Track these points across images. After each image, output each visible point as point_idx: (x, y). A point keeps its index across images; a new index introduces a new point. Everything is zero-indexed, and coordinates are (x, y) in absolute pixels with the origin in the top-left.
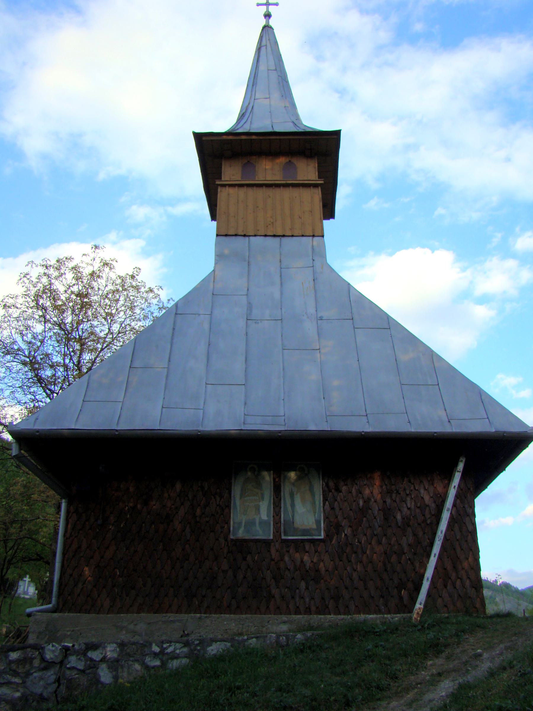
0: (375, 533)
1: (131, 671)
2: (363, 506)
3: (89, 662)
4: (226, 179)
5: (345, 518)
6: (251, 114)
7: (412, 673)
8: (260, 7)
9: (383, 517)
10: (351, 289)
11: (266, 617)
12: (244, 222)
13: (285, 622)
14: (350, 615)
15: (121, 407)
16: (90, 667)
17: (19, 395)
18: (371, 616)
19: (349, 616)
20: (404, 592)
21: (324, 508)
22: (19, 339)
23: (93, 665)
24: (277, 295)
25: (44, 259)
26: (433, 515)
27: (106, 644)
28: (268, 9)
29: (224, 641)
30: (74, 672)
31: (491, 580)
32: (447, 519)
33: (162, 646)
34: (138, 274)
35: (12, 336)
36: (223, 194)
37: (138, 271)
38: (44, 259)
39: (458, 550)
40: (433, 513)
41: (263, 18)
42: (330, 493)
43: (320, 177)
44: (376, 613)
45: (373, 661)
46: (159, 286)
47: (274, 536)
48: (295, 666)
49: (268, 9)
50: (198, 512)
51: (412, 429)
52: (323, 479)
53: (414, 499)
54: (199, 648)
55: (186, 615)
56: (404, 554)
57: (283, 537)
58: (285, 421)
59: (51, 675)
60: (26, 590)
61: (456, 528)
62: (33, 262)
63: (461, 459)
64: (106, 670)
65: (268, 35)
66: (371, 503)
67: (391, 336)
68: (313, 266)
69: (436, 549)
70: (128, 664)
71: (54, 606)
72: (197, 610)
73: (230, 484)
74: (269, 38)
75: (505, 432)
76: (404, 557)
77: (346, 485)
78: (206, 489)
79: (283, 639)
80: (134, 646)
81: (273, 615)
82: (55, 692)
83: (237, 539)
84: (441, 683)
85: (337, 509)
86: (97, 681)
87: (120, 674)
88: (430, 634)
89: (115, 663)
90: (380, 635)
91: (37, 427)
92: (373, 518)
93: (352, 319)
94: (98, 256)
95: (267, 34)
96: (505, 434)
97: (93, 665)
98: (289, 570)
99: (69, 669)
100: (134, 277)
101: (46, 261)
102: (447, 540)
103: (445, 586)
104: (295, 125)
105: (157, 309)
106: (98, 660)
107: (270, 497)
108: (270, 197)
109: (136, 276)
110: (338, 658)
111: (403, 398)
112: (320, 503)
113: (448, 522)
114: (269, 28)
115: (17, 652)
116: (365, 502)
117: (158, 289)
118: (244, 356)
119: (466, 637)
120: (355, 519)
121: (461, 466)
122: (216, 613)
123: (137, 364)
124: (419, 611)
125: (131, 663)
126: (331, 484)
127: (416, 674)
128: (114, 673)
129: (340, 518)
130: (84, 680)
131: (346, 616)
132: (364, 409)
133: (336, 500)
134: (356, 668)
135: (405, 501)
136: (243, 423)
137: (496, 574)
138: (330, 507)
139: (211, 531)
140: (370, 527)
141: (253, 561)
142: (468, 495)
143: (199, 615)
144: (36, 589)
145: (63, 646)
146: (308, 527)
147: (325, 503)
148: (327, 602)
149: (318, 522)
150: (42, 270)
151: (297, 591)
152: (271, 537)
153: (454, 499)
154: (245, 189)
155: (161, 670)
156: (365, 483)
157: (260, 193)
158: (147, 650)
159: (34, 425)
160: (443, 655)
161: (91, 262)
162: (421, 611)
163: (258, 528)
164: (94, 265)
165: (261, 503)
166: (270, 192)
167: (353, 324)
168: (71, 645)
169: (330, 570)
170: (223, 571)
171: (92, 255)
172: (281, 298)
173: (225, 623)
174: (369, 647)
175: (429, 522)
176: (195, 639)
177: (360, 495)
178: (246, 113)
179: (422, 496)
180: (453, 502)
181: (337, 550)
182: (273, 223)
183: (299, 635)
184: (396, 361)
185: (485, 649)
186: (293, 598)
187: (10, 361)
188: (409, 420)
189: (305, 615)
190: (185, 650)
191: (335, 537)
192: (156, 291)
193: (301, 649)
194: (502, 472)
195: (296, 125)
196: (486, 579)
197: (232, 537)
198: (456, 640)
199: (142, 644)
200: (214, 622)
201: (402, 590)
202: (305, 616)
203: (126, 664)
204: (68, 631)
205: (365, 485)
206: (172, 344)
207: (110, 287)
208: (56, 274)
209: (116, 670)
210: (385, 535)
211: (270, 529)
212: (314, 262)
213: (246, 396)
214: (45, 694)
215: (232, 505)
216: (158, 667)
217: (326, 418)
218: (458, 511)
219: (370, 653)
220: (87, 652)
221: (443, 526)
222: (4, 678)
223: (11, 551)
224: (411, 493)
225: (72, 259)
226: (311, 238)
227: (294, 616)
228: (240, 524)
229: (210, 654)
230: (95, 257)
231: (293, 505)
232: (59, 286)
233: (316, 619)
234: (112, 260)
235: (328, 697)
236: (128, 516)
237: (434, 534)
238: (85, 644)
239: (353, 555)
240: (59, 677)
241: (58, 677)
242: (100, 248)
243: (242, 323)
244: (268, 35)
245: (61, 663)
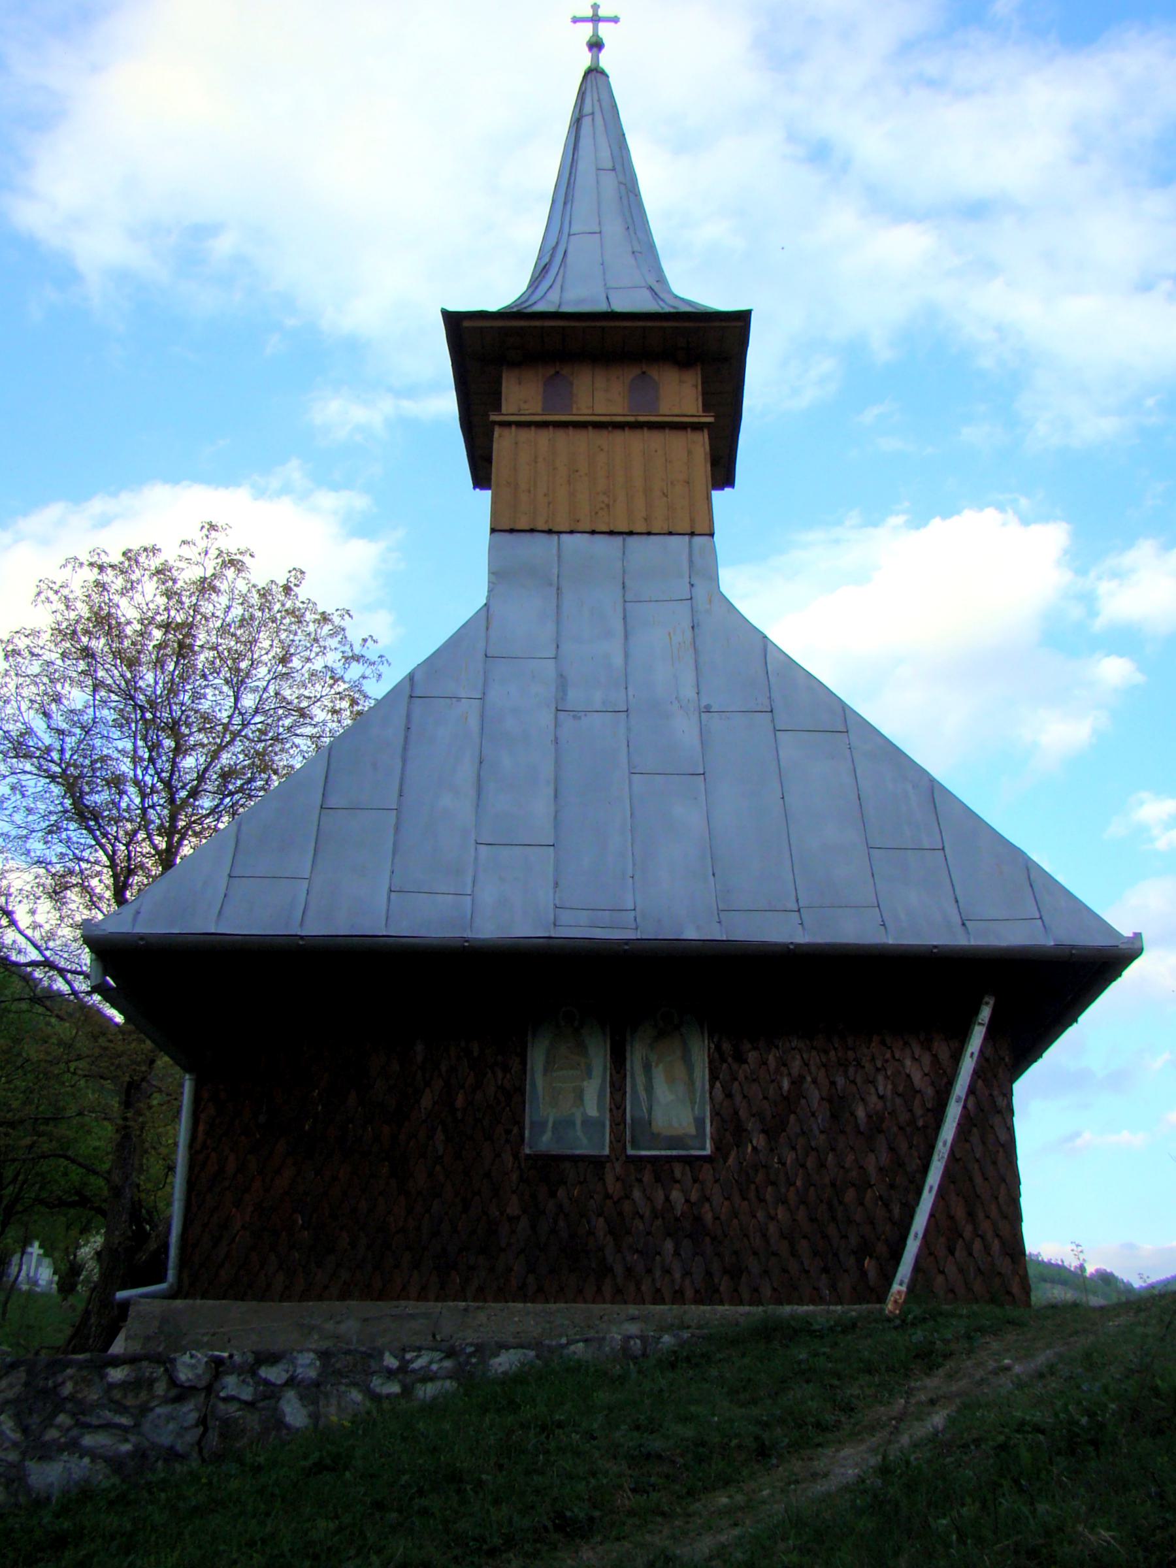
0: (813, 1144)
1: (343, 1404)
2: (789, 1091)
3: (261, 1388)
4: (511, 411)
5: (754, 1115)
6: (562, 269)
7: (881, 1402)
8: (579, 25)
9: (828, 1113)
10: (769, 648)
11: (597, 1308)
12: (549, 503)
13: (633, 1319)
14: (762, 1305)
15: (308, 891)
16: (266, 1398)
17: (36, 846)
18: (805, 1308)
19: (761, 1308)
20: (869, 1262)
21: (711, 1093)
22: (39, 724)
23: (271, 1392)
24: (618, 661)
25: (94, 551)
26: (928, 1110)
27: (295, 1354)
28: (595, 29)
29: (522, 1347)
31: (1070, 1266)
32: (955, 1118)
33: (404, 1357)
34: (298, 583)
35: (23, 716)
36: (503, 443)
37: (299, 577)
38: (94, 551)
39: (978, 1180)
40: (929, 1106)
41: (586, 49)
42: (725, 1065)
43: (706, 407)
44: (812, 1302)
45: (808, 1381)
46: (344, 609)
47: (612, 1149)
48: (661, 1391)
49: (595, 29)
50: (460, 1101)
51: (889, 939)
52: (711, 1037)
53: (891, 1078)
54: (474, 1360)
55: (439, 1304)
56: (871, 1186)
57: (630, 1152)
58: (635, 920)
59: (189, 1412)
60: (32, 1274)
61: (975, 1138)
62: (78, 559)
63: (986, 999)
64: (296, 1403)
65: (597, 88)
66: (806, 1086)
67: (850, 748)
68: (691, 599)
69: (934, 1178)
70: (338, 1390)
71: (171, 1286)
72: (461, 1296)
74: (599, 97)
75: (1073, 947)
76: (869, 1194)
77: (756, 1048)
78: (476, 1054)
79: (635, 1343)
80: (348, 1357)
81: (610, 1305)
82: (199, 1443)
83: (535, 1155)
84: (933, 1415)
85: (738, 1098)
86: (280, 1423)
87: (322, 1410)
88: (916, 1333)
89: (314, 1389)
90: (822, 1337)
91: (140, 929)
92: (809, 1114)
93: (772, 711)
94: (216, 545)
95: (595, 88)
96: (1074, 952)
97: (271, 1392)
99: (226, 1400)
100: (291, 589)
101: (98, 554)
102: (958, 1160)
103: (951, 1251)
104: (655, 294)
105: (339, 661)
106: (279, 1382)
108: (602, 450)
109: (295, 588)
110: (743, 1376)
111: (873, 875)
112: (703, 1086)
113: (959, 1124)
114: (599, 75)
115: (122, 1367)
116: (793, 1083)
117: (342, 616)
118: (552, 786)
119: (984, 1341)
120: (774, 1117)
121: (985, 1013)
122: (496, 1300)
123: (333, 801)
124: (898, 1297)
125: (343, 1388)
126: (726, 1046)
127: (889, 1403)
128: (311, 1408)
129: (743, 1114)
130: (253, 1421)
131: (755, 1308)
132: (793, 898)
133: (736, 1079)
134: (776, 1394)
135: (873, 1082)
136: (552, 926)
137: (1072, 1243)
138: (723, 1091)
140: (804, 1133)
141: (571, 1199)
142: (1000, 1071)
143: (464, 1304)
144: (55, 1273)
145: (212, 1356)
147: (715, 1083)
148: (716, 1281)
149: (699, 1122)
150: (93, 575)
151: (658, 1257)
152: (607, 1152)
153: (972, 1078)
155: (403, 1402)
156: (794, 1044)
157: (582, 441)
158: (374, 1365)
159: (134, 926)
160: (941, 1372)
161: (199, 559)
162: (903, 1296)
163: (579, 1133)
164: (205, 565)
165: (585, 1083)
166: (601, 439)
167: (773, 720)
168: (226, 1355)
169: (723, 1217)
170: (510, 1219)
171: (202, 544)
172: (626, 664)
173: (516, 1319)
174: (801, 1357)
175: (920, 1123)
176: (467, 1345)
177: (782, 1068)
178: (550, 265)
179: (908, 1071)
180: (968, 1084)
181: (736, 1178)
182: (608, 506)
183: (666, 1336)
184: (859, 799)
185: (1016, 1359)
186: (649, 1271)
187: (18, 771)
188: (883, 921)
189: (673, 1304)
190: (448, 1364)
191: (733, 1154)
192: (337, 620)
193: (672, 1362)
194: (1070, 1025)
195: (656, 294)
196: (1060, 1263)
197: (527, 1151)
198: (966, 1346)
199: (365, 1353)
200: (493, 1318)
201: (866, 1258)
202: (675, 1306)
203: (335, 1392)
204: (204, 1335)
205: (794, 1049)
206: (404, 760)
207: (237, 611)
208: (119, 583)
209: (315, 1402)
210: (833, 1149)
211: (603, 1135)
212: (694, 590)
213: (557, 869)
214: (179, 1447)
215: (528, 1087)
216: (397, 1395)
217: (718, 914)
218: (978, 1104)
219: (803, 1366)
220: (258, 1369)
221: (948, 1132)
222: (99, 1417)
223: (11, 1188)
224: (885, 1065)
225: (157, 550)
226: (687, 538)
227: (652, 1307)
228: (543, 1125)
229: (496, 1371)
230: (209, 546)
231: (649, 1089)
232: (127, 611)
233: (696, 1312)
234: (241, 553)
235: (726, 1440)
236: (320, 1108)
237: (931, 1147)
238: (253, 1352)
239: (770, 1189)
240: (205, 1415)
241: (202, 1415)
242: (221, 529)
243: (546, 718)
244: (597, 88)
245: (209, 1389)
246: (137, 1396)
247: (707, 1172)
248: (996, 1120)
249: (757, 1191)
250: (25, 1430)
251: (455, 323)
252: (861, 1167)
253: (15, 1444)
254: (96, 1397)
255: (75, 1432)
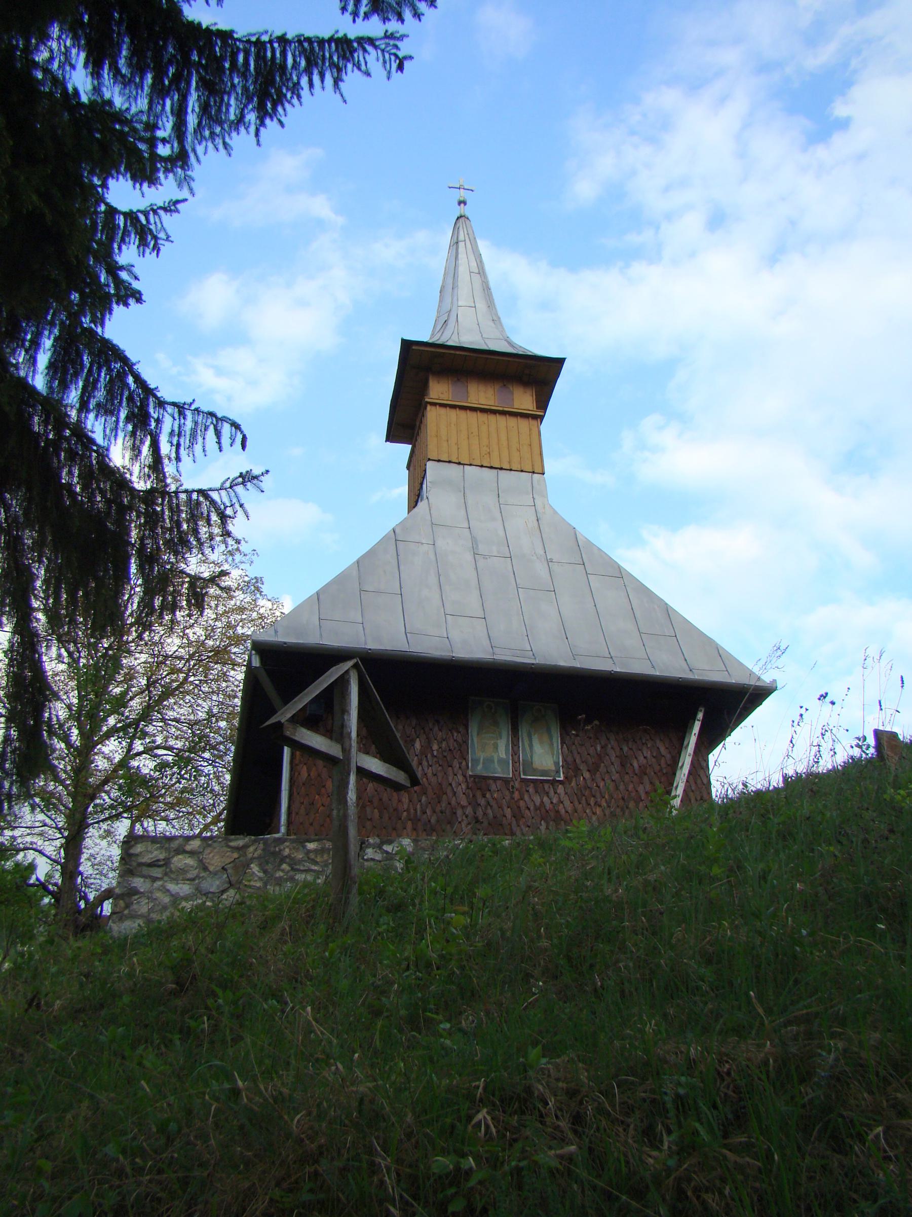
8: (346, 98)
16: (387, 859)
30: (371, 864)
56: (642, 800)
57: (523, 777)
73: (467, 721)
98: (529, 809)
99: (367, 860)
107: (508, 734)
112: (558, 746)
116: (602, 747)
121: (700, 715)
139: (449, 766)
146: (546, 769)
149: (556, 764)
152: (511, 776)
154: (458, 411)
157: (473, 417)
165: (499, 741)
166: (483, 417)
175: (665, 772)
191: (574, 779)
211: (509, 767)
231: (531, 746)
243: (469, 557)
246: (322, 856)
247: (560, 789)
248: (701, 773)
249: (586, 800)
250: (265, 872)
251: (407, 346)
252: (637, 791)
253: (260, 879)
254: (301, 857)
255: (292, 873)
